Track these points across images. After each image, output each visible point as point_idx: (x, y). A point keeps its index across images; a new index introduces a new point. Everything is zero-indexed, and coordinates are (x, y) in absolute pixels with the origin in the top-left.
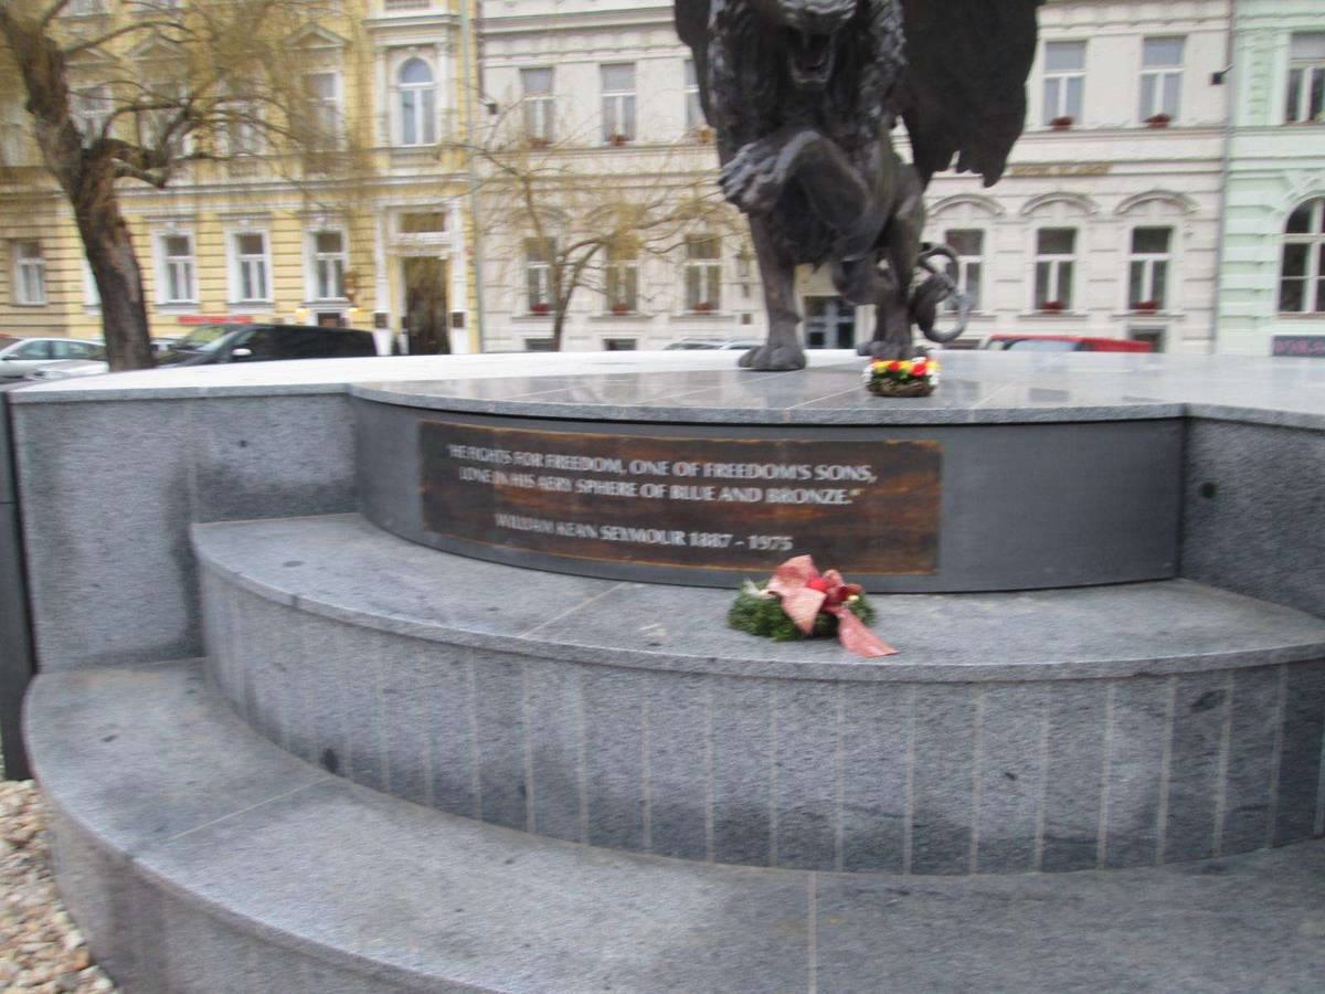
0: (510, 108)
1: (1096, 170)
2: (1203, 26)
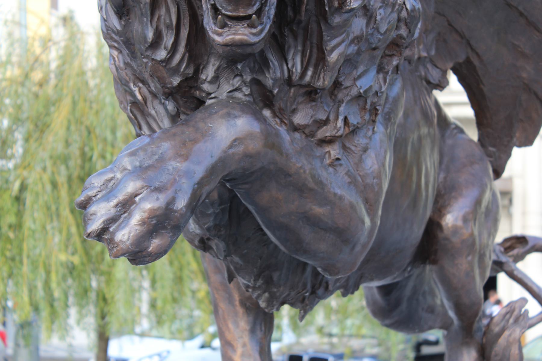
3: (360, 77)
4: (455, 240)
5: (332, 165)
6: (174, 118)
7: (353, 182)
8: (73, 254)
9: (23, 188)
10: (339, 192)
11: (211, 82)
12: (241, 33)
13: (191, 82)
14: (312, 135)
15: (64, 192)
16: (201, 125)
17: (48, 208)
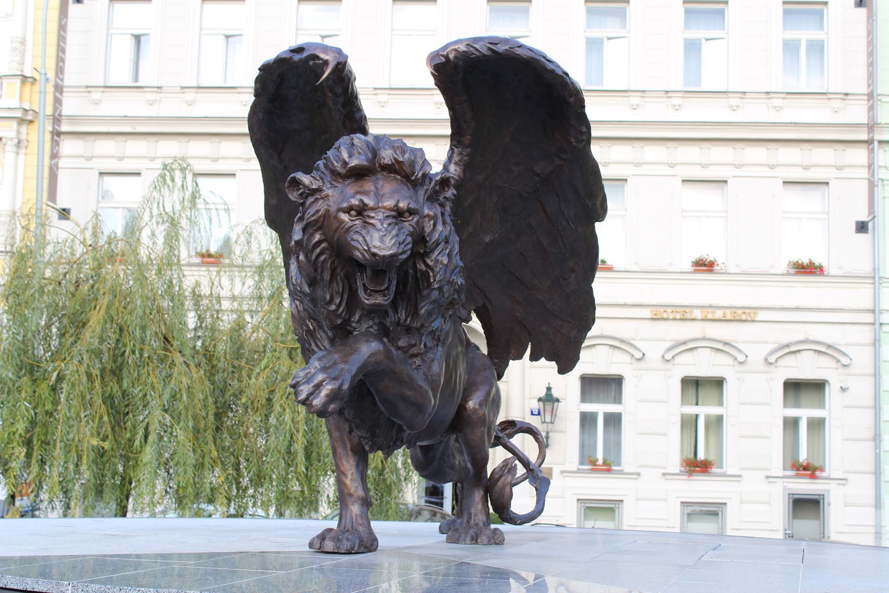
0: (117, 372)
1: (741, 316)
3: (433, 321)
4: (474, 417)
5: (416, 369)
6: (332, 341)
7: (426, 379)
8: (104, 440)
9: (60, 379)
10: (420, 383)
11: (357, 322)
12: (379, 300)
13: (347, 322)
14: (407, 352)
15: (97, 384)
16: (354, 345)
17: (83, 397)
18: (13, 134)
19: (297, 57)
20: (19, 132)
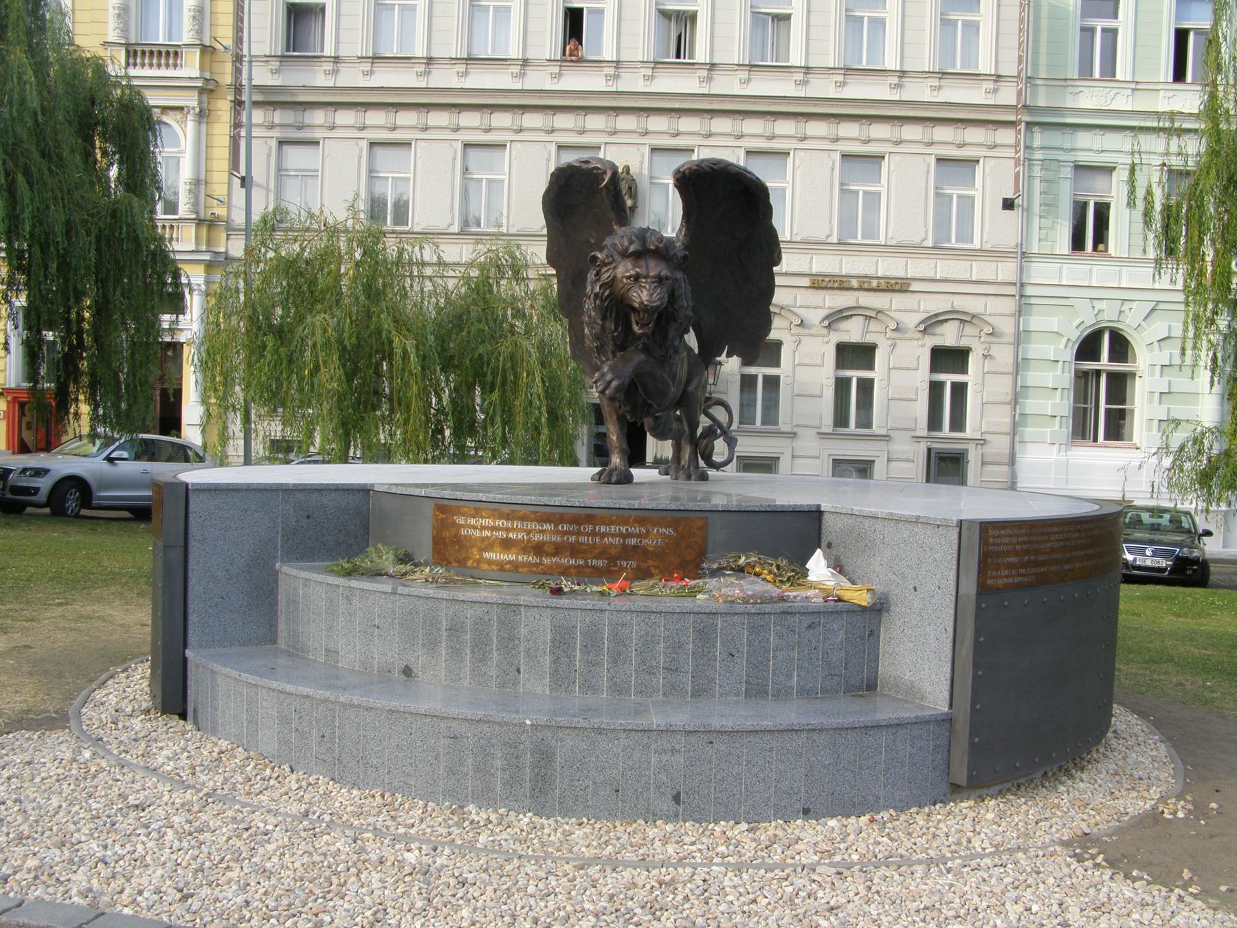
1: (898, 286)
2: (1139, 87)
18: (195, 104)
19: (584, 166)
20: (200, 102)
